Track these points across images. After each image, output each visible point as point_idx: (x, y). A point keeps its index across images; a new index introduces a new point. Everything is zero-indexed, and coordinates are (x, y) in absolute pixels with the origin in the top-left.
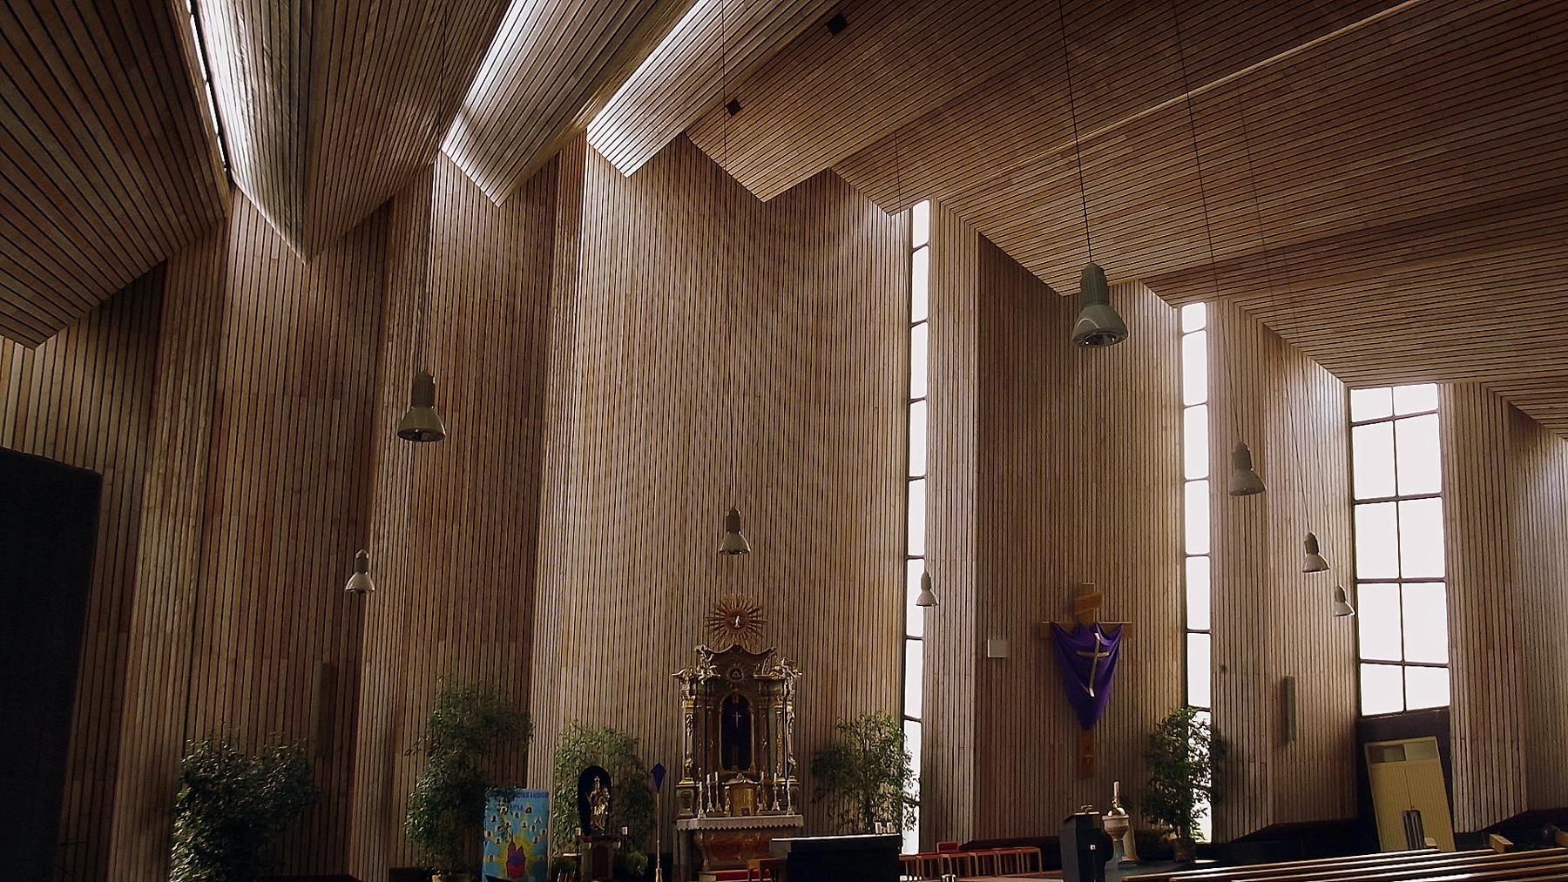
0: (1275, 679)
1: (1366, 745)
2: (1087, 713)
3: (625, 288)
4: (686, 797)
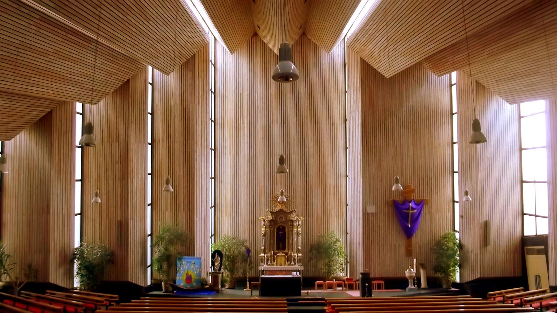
0: (481, 220)
1: (526, 248)
2: (409, 233)
3: (240, 91)
4: (262, 259)
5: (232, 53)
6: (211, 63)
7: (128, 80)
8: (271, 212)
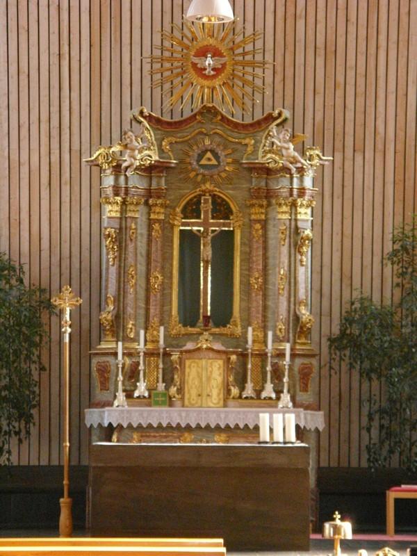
8: (150, 118)
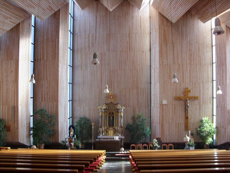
5: (82, 10)
6: (70, 16)
7: (19, 23)
